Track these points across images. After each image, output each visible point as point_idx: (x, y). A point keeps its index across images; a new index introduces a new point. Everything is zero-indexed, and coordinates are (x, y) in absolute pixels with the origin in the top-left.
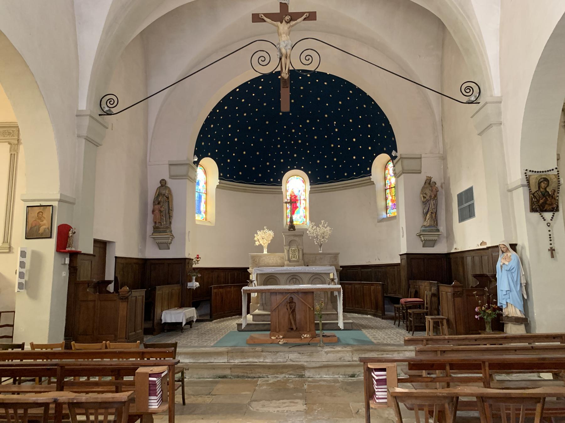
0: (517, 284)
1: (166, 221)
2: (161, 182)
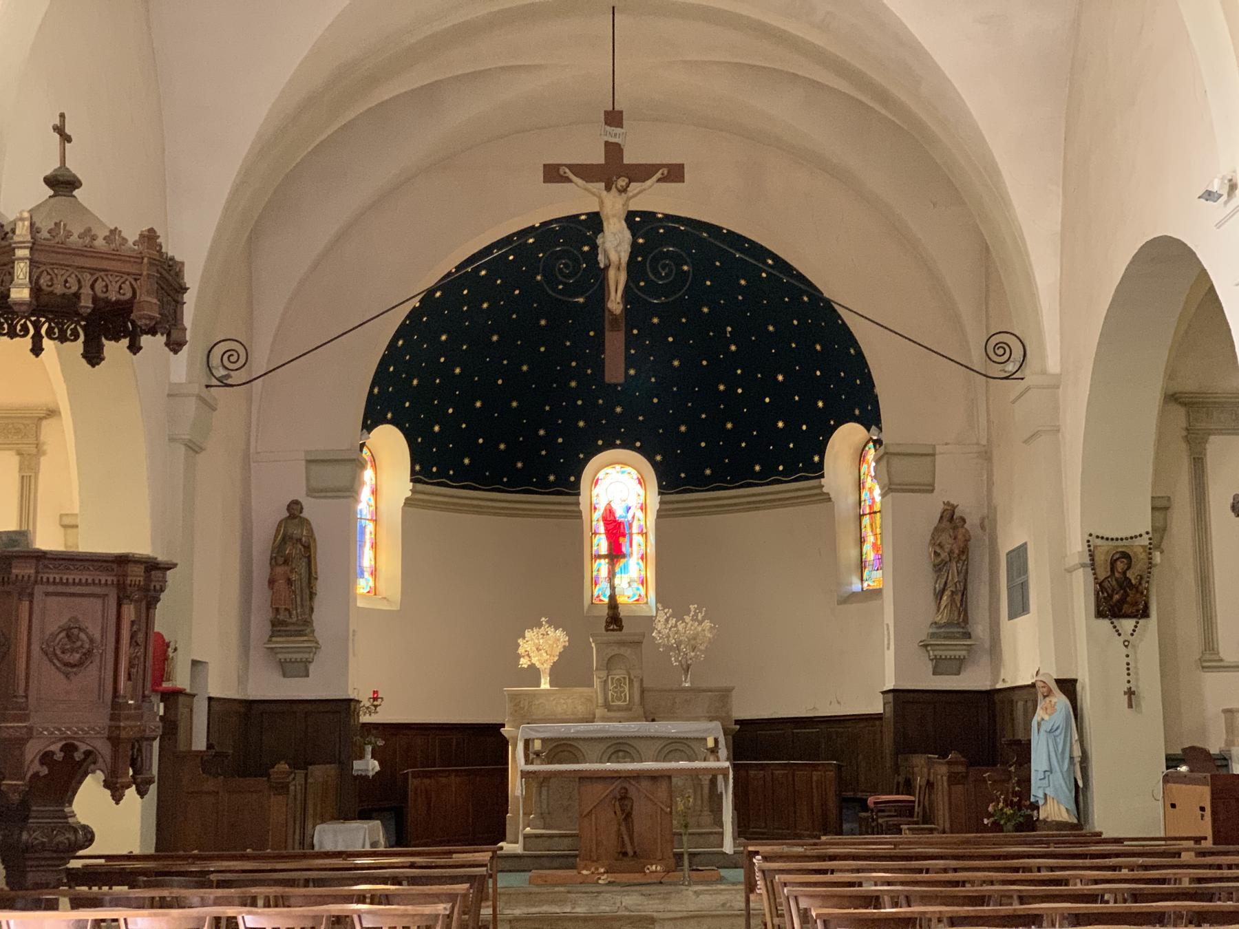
0: (1063, 758)
1: (302, 606)
2: (289, 507)
